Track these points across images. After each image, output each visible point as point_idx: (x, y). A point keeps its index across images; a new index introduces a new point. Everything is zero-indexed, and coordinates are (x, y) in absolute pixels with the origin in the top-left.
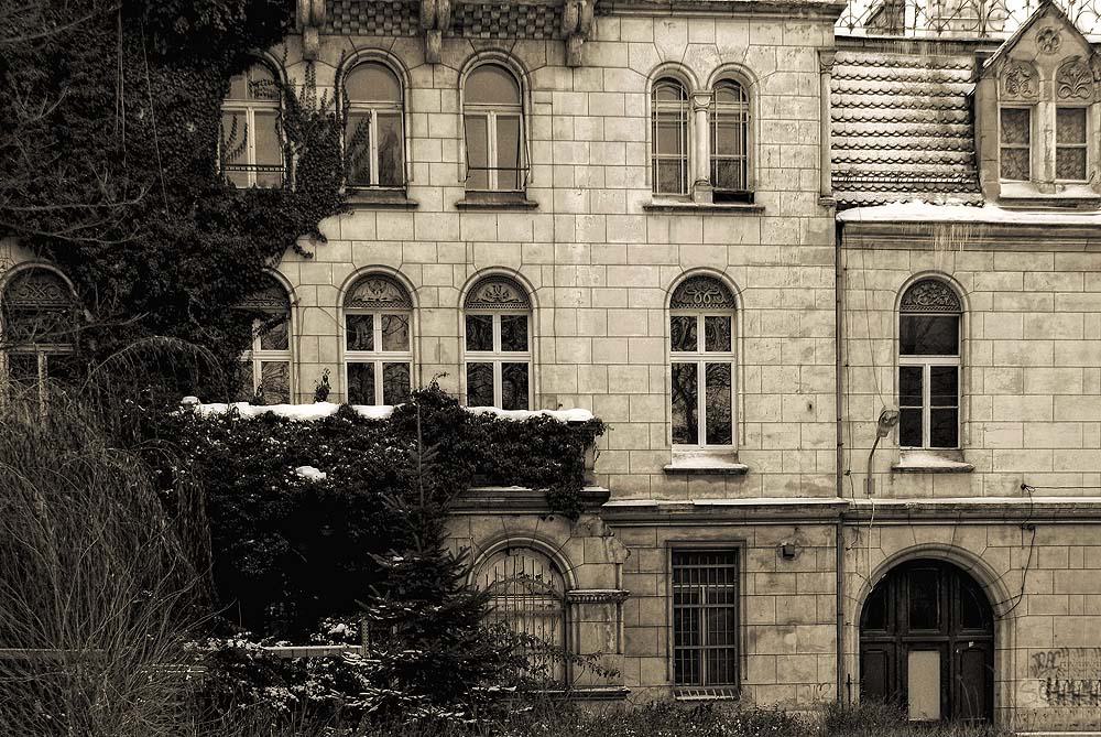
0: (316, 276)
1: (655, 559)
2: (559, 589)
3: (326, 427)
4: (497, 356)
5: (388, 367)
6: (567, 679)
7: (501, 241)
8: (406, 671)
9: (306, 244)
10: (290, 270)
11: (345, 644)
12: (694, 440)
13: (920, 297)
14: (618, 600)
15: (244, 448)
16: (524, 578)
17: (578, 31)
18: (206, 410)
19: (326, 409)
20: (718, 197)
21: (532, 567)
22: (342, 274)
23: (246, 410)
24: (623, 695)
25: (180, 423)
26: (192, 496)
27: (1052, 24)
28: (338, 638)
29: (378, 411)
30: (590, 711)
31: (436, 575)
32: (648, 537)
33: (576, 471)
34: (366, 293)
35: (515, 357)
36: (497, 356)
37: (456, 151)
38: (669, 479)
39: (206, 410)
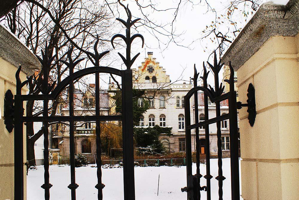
0: (146, 115)
1: (177, 139)
2: (168, 142)
3: (147, 129)
4: (163, 121)
5: (164, 123)
6: (169, 151)
7: (163, 112)
8: (155, 150)
9: (145, 112)
10: (144, 114)
11: (149, 148)
12: (181, 128)
13: (201, 115)
14: (174, 143)
15: (140, 130)
16: (165, 141)
17: (170, 93)
18: (137, 127)
19: (148, 127)
20: (182, 107)
21: (166, 140)
22: (149, 114)
23: (140, 127)
24: (175, 152)
25: (135, 128)
26: (136, 135)
27: (142, 79)
28: (149, 147)
29: (152, 127)
30: (171, 153)
31: (158, 142)
32: (177, 137)
33: (170, 132)
34: (151, 116)
35: (164, 121)
36: (152, 122)
37: (273, 110)
38: (77, 144)
39: (137, 127)
